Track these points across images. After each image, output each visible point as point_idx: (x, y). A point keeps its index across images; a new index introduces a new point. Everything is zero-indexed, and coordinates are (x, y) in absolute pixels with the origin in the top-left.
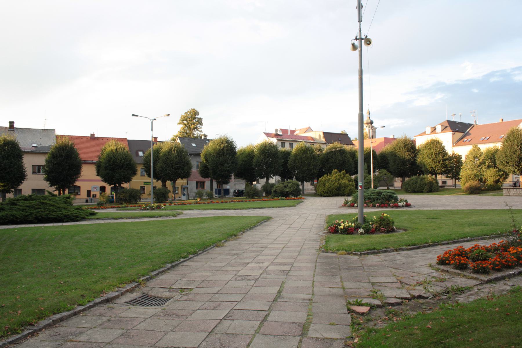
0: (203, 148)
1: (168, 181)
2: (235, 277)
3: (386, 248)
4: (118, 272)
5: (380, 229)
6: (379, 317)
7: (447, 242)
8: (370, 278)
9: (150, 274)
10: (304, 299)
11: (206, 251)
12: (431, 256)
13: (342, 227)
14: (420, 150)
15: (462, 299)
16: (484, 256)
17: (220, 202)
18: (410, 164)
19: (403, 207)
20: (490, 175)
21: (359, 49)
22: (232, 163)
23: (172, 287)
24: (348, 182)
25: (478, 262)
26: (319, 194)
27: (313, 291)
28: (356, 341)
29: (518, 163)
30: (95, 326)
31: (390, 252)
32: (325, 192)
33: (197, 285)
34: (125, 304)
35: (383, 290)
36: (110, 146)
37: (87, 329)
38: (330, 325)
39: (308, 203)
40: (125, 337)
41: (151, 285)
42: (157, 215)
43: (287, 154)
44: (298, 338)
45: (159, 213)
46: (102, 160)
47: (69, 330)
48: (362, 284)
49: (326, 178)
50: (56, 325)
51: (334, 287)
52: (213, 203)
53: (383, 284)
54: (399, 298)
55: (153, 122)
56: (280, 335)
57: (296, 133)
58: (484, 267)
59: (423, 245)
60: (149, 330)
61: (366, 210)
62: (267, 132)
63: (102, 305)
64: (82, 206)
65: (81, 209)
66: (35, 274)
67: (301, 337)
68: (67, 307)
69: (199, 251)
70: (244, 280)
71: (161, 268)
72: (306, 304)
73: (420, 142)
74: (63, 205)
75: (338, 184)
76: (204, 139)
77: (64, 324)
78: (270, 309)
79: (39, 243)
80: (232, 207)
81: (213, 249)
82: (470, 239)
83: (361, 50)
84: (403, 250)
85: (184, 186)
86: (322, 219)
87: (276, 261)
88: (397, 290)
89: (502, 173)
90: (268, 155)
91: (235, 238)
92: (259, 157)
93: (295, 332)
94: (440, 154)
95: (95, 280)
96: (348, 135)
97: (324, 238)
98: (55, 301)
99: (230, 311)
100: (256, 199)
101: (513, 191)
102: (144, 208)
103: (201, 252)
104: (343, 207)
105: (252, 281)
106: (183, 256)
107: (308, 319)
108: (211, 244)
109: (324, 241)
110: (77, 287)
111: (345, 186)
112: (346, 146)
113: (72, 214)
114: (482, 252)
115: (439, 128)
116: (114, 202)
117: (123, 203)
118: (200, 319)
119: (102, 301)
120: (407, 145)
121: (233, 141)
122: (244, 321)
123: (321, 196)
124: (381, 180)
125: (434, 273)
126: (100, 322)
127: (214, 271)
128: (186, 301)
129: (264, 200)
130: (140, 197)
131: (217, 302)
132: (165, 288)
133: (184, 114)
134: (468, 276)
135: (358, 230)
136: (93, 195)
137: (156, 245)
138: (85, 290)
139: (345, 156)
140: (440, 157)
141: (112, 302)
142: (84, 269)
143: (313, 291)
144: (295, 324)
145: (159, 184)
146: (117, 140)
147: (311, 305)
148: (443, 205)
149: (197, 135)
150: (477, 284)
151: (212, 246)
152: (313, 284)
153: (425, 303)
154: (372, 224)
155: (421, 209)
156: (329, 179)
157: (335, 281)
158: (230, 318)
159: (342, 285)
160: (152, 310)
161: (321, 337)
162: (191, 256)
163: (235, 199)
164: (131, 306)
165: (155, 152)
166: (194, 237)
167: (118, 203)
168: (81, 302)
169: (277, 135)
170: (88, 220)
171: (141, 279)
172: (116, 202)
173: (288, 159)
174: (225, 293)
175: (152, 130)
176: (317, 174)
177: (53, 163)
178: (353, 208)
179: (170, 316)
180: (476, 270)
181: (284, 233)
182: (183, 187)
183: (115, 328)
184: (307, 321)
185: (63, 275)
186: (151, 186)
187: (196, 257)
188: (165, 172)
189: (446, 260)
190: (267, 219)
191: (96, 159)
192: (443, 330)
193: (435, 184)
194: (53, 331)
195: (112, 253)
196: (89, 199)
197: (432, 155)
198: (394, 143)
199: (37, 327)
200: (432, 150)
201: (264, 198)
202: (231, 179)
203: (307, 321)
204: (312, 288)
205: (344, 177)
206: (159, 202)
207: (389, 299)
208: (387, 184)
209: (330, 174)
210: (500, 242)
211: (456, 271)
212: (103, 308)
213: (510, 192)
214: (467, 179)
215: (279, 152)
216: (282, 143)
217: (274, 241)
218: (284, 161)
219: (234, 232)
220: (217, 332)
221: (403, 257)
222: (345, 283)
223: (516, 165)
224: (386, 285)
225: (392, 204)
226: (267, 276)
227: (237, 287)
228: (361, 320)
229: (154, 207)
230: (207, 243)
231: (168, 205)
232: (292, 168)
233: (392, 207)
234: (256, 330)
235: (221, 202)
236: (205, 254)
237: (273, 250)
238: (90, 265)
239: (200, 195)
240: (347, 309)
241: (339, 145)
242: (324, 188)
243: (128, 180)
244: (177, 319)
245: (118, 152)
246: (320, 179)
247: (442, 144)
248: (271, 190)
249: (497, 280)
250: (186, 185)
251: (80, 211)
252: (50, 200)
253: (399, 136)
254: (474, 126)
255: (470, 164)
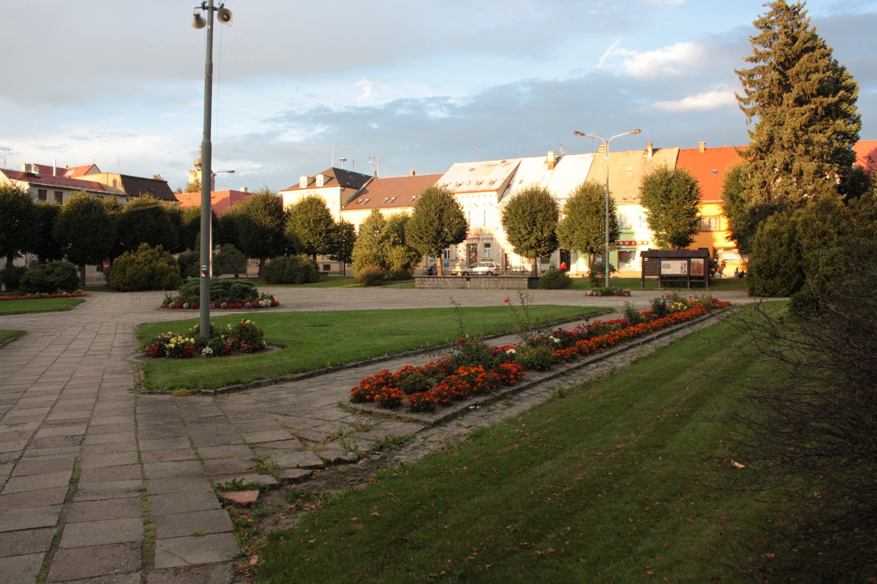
3: (258, 379)
5: (239, 347)
6: (279, 506)
7: (354, 364)
8: (244, 435)
10: (128, 491)
12: (336, 388)
13: (173, 346)
14: (290, 214)
15: (404, 456)
16: (423, 384)
19: (266, 307)
20: (396, 256)
21: (207, 27)
24: (167, 265)
27: (143, 472)
28: (253, 562)
31: (265, 386)
32: (126, 282)
35: (273, 456)
38: (193, 537)
39: (96, 304)
43: (51, 213)
48: (231, 448)
49: (128, 257)
51: (180, 459)
53: (270, 444)
54: (305, 468)
56: (95, 577)
57: (68, 174)
58: (428, 401)
61: (213, 314)
62: (7, 168)
72: (134, 499)
73: (290, 200)
78: (61, 522)
82: (389, 357)
84: (286, 380)
86: (127, 331)
87: (52, 417)
88: (296, 453)
89: (414, 253)
96: (166, 182)
97: (141, 367)
101: (429, 282)
104: (162, 309)
105: (6, 466)
109: (141, 372)
112: (164, 202)
115: (320, 179)
120: (269, 204)
122: (5, 559)
123: (118, 289)
124: (225, 263)
125: (350, 418)
134: (405, 418)
143: (143, 472)
144: (122, 546)
150: (420, 429)
152: (139, 457)
153: (348, 471)
154: (226, 338)
155: (298, 310)
156: (133, 260)
157: (180, 447)
159: (196, 454)
161: (182, 564)
169: (28, 176)
173: (53, 222)
178: (181, 310)
181: (58, 360)
184: (146, 537)
189: (366, 394)
190: (18, 335)
193: (313, 269)
198: (248, 201)
200: (310, 215)
201: (4, 295)
203: (146, 537)
204: (140, 465)
205: (160, 256)
207: (288, 471)
208: (235, 269)
209: (135, 251)
210: (439, 360)
213: (424, 283)
214: (362, 262)
216: (40, 191)
217: (39, 378)
221: (290, 393)
222: (200, 450)
223: (433, 242)
224: (274, 445)
225: (248, 303)
226: (39, 450)
228: (249, 518)
233: (249, 308)
234: (39, 575)
237: (42, 396)
240: (218, 500)
241: (152, 200)
246: (116, 259)
247: (325, 205)
249: (447, 419)
253: (255, 189)
254: (373, 180)
255: (368, 239)
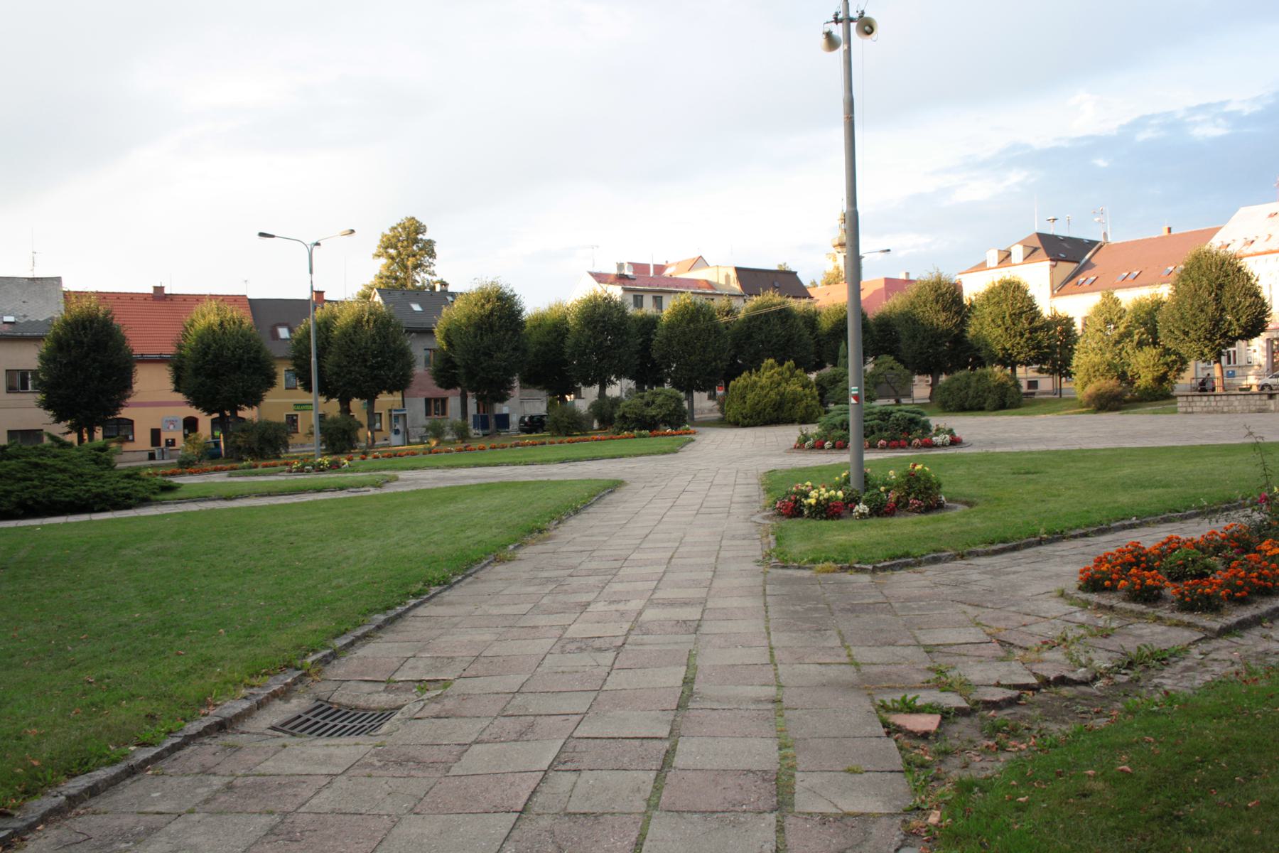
0: (439, 313)
1: (355, 400)
2: (560, 644)
3: (935, 551)
4: (245, 644)
5: (907, 504)
7: (1082, 531)
8: (917, 633)
9: (331, 646)
10: (758, 701)
11: (470, 575)
13: (813, 501)
14: (975, 307)
15: (1169, 680)
16: (1199, 566)
17: (488, 447)
18: (950, 342)
19: (944, 445)
20: (1144, 364)
21: (843, 47)
22: (515, 349)
23: (392, 678)
24: (801, 389)
25: (1190, 582)
26: (732, 420)
29: (1210, 333)
30: (189, 807)
31: (945, 561)
33: (461, 671)
34: (270, 732)
35: (960, 665)
36: (204, 316)
37: (168, 816)
38: (847, 774)
40: (282, 837)
41: (336, 675)
42: (333, 486)
43: (649, 324)
44: (772, 818)
45: (337, 480)
46: (186, 352)
47: (117, 823)
48: (899, 651)
49: (748, 380)
50: (78, 810)
52: (471, 450)
54: (1009, 687)
55: (312, 250)
56: (717, 812)
57: (667, 272)
58: (1208, 594)
59: (1026, 541)
60: (345, 814)
61: (869, 456)
62: (596, 270)
63: (206, 740)
64: (140, 468)
65: (137, 476)
66: (16, 660)
67: (777, 813)
68: (108, 753)
69: (454, 575)
70: (585, 650)
71: (358, 625)
72: (766, 712)
73: (973, 288)
74: (90, 468)
75: (778, 394)
76: (442, 291)
77: (100, 803)
78: (674, 734)
79: (28, 571)
80: (520, 460)
81: (489, 568)
82: (1138, 522)
83: (849, 48)
84: (978, 554)
85: (395, 410)
87: (659, 595)
88: (996, 664)
89: (1174, 357)
90: (602, 327)
91: (541, 536)
92: (580, 332)
93: (758, 799)
94: (1023, 315)
95: (184, 668)
96: (795, 273)
97: (771, 530)
98: (72, 738)
99: (565, 743)
100: (577, 438)
101: (1201, 402)
102: (298, 468)
103: (460, 578)
104: (795, 451)
106: (414, 590)
107: (784, 757)
108: (483, 555)
109: (771, 538)
110: (134, 693)
111: (794, 399)
113: (114, 490)
114: (1193, 556)
115: (1018, 253)
116: (221, 454)
117: (245, 458)
118: (485, 771)
119: (205, 727)
120: (943, 295)
121: (515, 295)
122: (610, 772)
123: (736, 424)
124: (882, 382)
126: (203, 792)
127: (500, 630)
128: (438, 717)
129: (597, 440)
130: (287, 442)
131: (523, 718)
132: (376, 681)
133: (387, 232)
134: (1169, 619)
135: (852, 508)
136: (167, 440)
137: (339, 562)
138: (157, 699)
139: (792, 326)
140: (1024, 323)
141: (233, 728)
142: (151, 638)
145: (333, 407)
146: (223, 300)
147: (782, 716)
148: (1039, 440)
149: (423, 283)
150: (1196, 638)
151: (485, 562)
152: (772, 655)
154: (887, 491)
155: (991, 450)
156: (755, 383)
158: (569, 766)
159: (849, 656)
160: (346, 748)
161: (830, 810)
162: (433, 590)
163: (525, 438)
164: (287, 739)
165: (320, 328)
166: (435, 539)
167: (231, 457)
168: (147, 737)
169: (621, 278)
170: (157, 504)
171: (309, 660)
172: (226, 457)
173: (652, 336)
174: (540, 689)
175: (311, 272)
176: (723, 372)
177: (60, 363)
178: (821, 451)
179: (401, 765)
180: (1186, 602)
182: (394, 413)
183: (249, 810)
185: (95, 656)
186: (313, 413)
187: (447, 593)
188: (348, 376)
190: (614, 486)
191: (170, 350)
192: (1166, 779)
193: (1012, 388)
194: (69, 828)
195: (224, 591)
196: (157, 451)
197: (1004, 318)
198: (911, 291)
199: (20, 820)
200: (1004, 306)
201: (597, 434)
202: (511, 388)
204: (774, 667)
205: (792, 376)
206: (336, 453)
207: (983, 689)
209: (757, 370)
211: (1133, 606)
212: (212, 749)
213: (1193, 404)
214: (1089, 375)
215: (630, 318)
216: (635, 297)
218: (643, 342)
219: (537, 522)
220: (541, 811)
222: (854, 651)
224: (963, 650)
225: (917, 441)
226: (645, 637)
227: (570, 673)
228: (926, 754)
229: (323, 464)
230: (470, 552)
231: (357, 458)
232: (663, 357)
233: (918, 447)
234: (649, 799)
235: (491, 448)
236: (471, 583)
237: (646, 565)
238: (167, 625)
239: (437, 432)
240: (880, 725)
241: (777, 299)
242: (743, 405)
243: (254, 399)
244: (420, 774)
245: (225, 329)
246: (732, 383)
247: (1026, 291)
248: (612, 414)
249: (1244, 625)
250: (401, 408)
251: (136, 483)
252: (55, 456)
253: (921, 273)
254: (1101, 246)
255: (1097, 339)
